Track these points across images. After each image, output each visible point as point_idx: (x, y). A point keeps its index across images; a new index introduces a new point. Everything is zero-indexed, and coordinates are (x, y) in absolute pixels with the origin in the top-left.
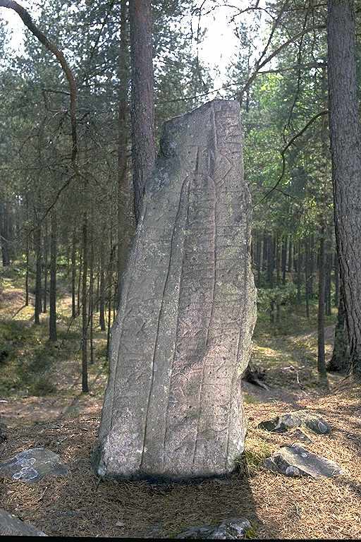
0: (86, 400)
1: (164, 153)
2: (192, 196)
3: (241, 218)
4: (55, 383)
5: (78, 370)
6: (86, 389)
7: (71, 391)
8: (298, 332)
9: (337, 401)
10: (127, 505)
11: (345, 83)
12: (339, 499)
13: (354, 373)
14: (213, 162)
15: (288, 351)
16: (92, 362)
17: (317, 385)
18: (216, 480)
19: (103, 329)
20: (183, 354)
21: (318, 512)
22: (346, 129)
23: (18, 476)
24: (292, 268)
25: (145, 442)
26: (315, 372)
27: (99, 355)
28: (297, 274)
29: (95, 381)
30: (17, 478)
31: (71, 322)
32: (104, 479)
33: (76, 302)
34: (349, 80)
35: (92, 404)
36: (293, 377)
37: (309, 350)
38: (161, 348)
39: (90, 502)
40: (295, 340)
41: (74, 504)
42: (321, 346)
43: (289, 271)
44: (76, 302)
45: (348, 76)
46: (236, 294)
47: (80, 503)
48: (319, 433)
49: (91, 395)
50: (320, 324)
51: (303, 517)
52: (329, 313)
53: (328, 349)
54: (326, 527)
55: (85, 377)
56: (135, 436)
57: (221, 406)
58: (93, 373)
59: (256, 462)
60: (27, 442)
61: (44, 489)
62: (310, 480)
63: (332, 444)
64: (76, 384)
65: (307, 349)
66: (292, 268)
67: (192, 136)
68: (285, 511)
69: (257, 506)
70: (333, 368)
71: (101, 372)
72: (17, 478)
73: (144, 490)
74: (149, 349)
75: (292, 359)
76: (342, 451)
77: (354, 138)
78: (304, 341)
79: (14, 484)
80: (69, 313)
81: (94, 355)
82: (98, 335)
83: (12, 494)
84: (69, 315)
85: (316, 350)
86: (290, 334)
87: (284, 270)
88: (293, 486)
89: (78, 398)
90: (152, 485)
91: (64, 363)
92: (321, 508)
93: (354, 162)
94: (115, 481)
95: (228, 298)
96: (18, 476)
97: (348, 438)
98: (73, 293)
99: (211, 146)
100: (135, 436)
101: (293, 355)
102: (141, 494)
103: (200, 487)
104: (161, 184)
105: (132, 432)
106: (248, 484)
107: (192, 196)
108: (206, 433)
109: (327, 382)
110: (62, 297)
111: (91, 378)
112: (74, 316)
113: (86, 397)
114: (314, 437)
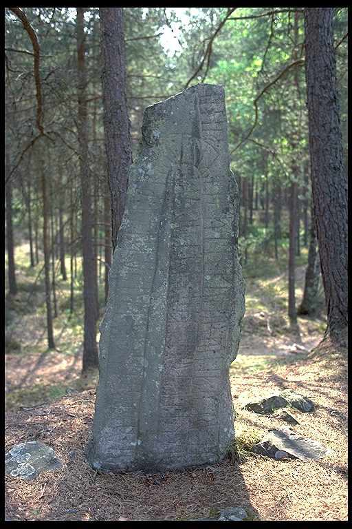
0: (54, 357)
1: (146, 141)
2: (177, 188)
3: (228, 210)
4: (19, 340)
5: (42, 325)
6: (52, 345)
7: (36, 347)
8: (268, 274)
9: (316, 370)
10: (126, 497)
11: (322, 34)
12: (326, 482)
13: (331, 335)
14: (198, 151)
15: (257, 296)
16: (56, 316)
17: (287, 331)
18: (209, 467)
19: (65, 278)
20: (173, 350)
21: (308, 496)
22: (324, 83)
23: (16, 473)
24: (259, 204)
25: (139, 435)
26: (286, 317)
27: (63, 307)
28: (264, 211)
29: (60, 335)
30: (15, 476)
31: (29, 271)
32: (100, 472)
33: (34, 250)
34: (326, 30)
35: (60, 361)
36: (263, 324)
37: (278, 294)
38: (151, 344)
39: (90, 497)
40: (264, 284)
41: (73, 500)
42: (292, 293)
43: (257, 209)
44: (34, 250)
45: (326, 25)
46: (224, 288)
47: (81, 498)
48: (304, 412)
49: (58, 351)
50: (291, 265)
51: (295, 502)
52: (299, 254)
53: (299, 293)
54: (317, 511)
55: (50, 333)
56: (128, 430)
57: (212, 397)
58: (58, 327)
59: (246, 448)
60: (16, 433)
61: (43, 485)
62: (298, 463)
63: (317, 423)
64: (41, 340)
65: (277, 293)
66: (259, 204)
67: (176, 124)
68: (277, 497)
69: (251, 493)
70: (304, 312)
71: (66, 326)
72: (15, 476)
73: (140, 481)
74: (138, 346)
75: (262, 303)
76: (326, 430)
77: (331, 93)
78: (274, 284)
79: (13, 482)
80: (26, 261)
81: (58, 309)
82: (62, 287)
83: (12, 492)
84: (28, 264)
85: (286, 295)
86: (259, 277)
87: (251, 209)
88: (282, 470)
89: (44, 354)
90: (148, 475)
91: (26, 318)
92: (310, 492)
93: (331, 119)
94: (111, 474)
95: (217, 291)
96: (16, 473)
97: (332, 416)
98: (29, 238)
99: (196, 134)
100: (128, 430)
101: (262, 299)
102: (137, 485)
103: (194, 475)
104: (146, 175)
105: (125, 426)
106: (240, 470)
107: (177, 188)
108: (199, 424)
109: (298, 328)
110: (19, 244)
111: (56, 333)
112: (32, 265)
113: (52, 353)
114: (299, 416)
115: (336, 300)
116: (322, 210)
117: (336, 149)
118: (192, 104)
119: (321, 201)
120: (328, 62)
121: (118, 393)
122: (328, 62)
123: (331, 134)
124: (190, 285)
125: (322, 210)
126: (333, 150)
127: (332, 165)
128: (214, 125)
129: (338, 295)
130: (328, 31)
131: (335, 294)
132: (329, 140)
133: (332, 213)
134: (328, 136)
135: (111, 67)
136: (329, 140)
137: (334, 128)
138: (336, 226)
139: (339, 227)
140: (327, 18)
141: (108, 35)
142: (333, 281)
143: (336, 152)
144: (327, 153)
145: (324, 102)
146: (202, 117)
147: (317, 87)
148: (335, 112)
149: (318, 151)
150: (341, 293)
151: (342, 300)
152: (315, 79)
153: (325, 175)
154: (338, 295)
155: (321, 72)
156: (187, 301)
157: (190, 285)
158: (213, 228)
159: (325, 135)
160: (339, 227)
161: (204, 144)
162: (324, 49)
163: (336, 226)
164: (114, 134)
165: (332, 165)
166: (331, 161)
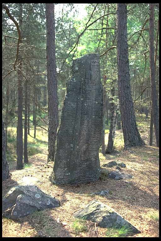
56: (66, 169)
100: (66, 169)
105: (65, 168)
115: (128, 137)
116: (122, 102)
117: (128, 80)
118: (89, 59)
119: (122, 99)
120: (125, 48)
121: (63, 156)
122: (125, 48)
123: (126, 74)
124: (88, 119)
125: (122, 102)
126: (127, 80)
127: (127, 86)
128: (96, 67)
129: (129, 135)
130: (125, 37)
131: (127, 135)
132: (125, 77)
133: (126, 104)
134: (125, 75)
135: (50, 45)
136: (125, 77)
137: (128, 72)
138: (128, 109)
139: (129, 109)
140: (125, 32)
141: (50, 34)
142: (126, 129)
143: (128, 81)
144: (124, 81)
145: (124, 63)
146: (92, 64)
147: (121, 57)
148: (128, 66)
149: (121, 80)
150: (130, 134)
151: (130, 137)
152: (120, 54)
153: (124, 90)
154: (129, 135)
155: (122, 51)
156: (87, 124)
157: (88, 119)
158: (95, 100)
159: (124, 75)
160: (129, 109)
161: (93, 73)
162: (124, 43)
163: (128, 109)
164: (51, 70)
165: (127, 86)
166: (126, 85)
